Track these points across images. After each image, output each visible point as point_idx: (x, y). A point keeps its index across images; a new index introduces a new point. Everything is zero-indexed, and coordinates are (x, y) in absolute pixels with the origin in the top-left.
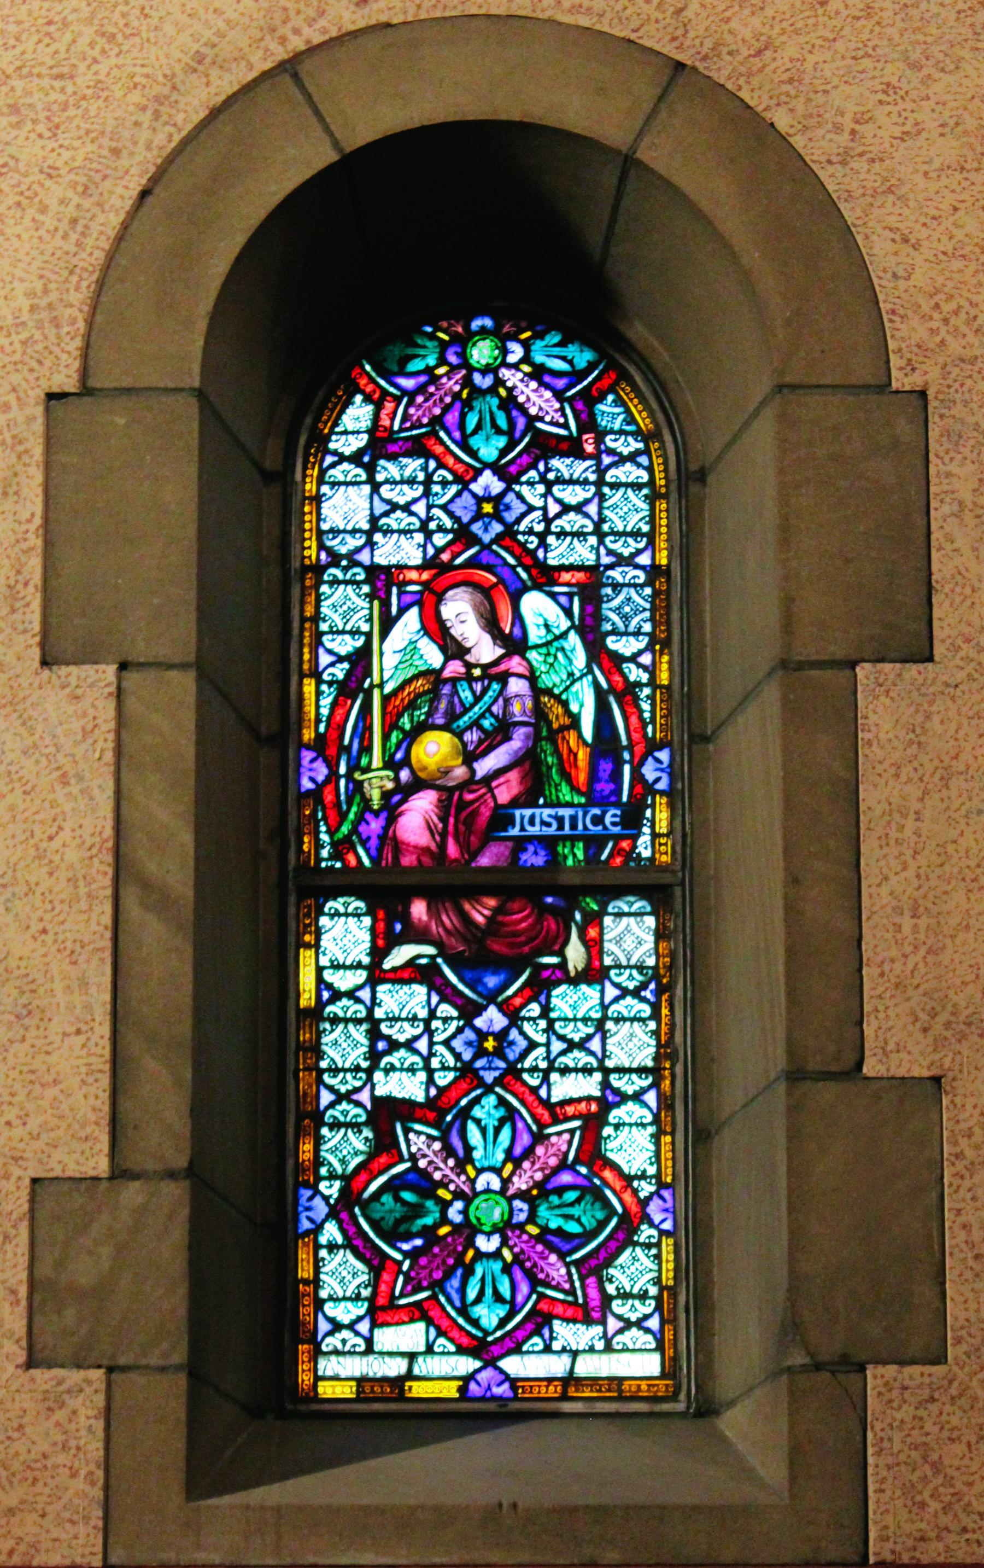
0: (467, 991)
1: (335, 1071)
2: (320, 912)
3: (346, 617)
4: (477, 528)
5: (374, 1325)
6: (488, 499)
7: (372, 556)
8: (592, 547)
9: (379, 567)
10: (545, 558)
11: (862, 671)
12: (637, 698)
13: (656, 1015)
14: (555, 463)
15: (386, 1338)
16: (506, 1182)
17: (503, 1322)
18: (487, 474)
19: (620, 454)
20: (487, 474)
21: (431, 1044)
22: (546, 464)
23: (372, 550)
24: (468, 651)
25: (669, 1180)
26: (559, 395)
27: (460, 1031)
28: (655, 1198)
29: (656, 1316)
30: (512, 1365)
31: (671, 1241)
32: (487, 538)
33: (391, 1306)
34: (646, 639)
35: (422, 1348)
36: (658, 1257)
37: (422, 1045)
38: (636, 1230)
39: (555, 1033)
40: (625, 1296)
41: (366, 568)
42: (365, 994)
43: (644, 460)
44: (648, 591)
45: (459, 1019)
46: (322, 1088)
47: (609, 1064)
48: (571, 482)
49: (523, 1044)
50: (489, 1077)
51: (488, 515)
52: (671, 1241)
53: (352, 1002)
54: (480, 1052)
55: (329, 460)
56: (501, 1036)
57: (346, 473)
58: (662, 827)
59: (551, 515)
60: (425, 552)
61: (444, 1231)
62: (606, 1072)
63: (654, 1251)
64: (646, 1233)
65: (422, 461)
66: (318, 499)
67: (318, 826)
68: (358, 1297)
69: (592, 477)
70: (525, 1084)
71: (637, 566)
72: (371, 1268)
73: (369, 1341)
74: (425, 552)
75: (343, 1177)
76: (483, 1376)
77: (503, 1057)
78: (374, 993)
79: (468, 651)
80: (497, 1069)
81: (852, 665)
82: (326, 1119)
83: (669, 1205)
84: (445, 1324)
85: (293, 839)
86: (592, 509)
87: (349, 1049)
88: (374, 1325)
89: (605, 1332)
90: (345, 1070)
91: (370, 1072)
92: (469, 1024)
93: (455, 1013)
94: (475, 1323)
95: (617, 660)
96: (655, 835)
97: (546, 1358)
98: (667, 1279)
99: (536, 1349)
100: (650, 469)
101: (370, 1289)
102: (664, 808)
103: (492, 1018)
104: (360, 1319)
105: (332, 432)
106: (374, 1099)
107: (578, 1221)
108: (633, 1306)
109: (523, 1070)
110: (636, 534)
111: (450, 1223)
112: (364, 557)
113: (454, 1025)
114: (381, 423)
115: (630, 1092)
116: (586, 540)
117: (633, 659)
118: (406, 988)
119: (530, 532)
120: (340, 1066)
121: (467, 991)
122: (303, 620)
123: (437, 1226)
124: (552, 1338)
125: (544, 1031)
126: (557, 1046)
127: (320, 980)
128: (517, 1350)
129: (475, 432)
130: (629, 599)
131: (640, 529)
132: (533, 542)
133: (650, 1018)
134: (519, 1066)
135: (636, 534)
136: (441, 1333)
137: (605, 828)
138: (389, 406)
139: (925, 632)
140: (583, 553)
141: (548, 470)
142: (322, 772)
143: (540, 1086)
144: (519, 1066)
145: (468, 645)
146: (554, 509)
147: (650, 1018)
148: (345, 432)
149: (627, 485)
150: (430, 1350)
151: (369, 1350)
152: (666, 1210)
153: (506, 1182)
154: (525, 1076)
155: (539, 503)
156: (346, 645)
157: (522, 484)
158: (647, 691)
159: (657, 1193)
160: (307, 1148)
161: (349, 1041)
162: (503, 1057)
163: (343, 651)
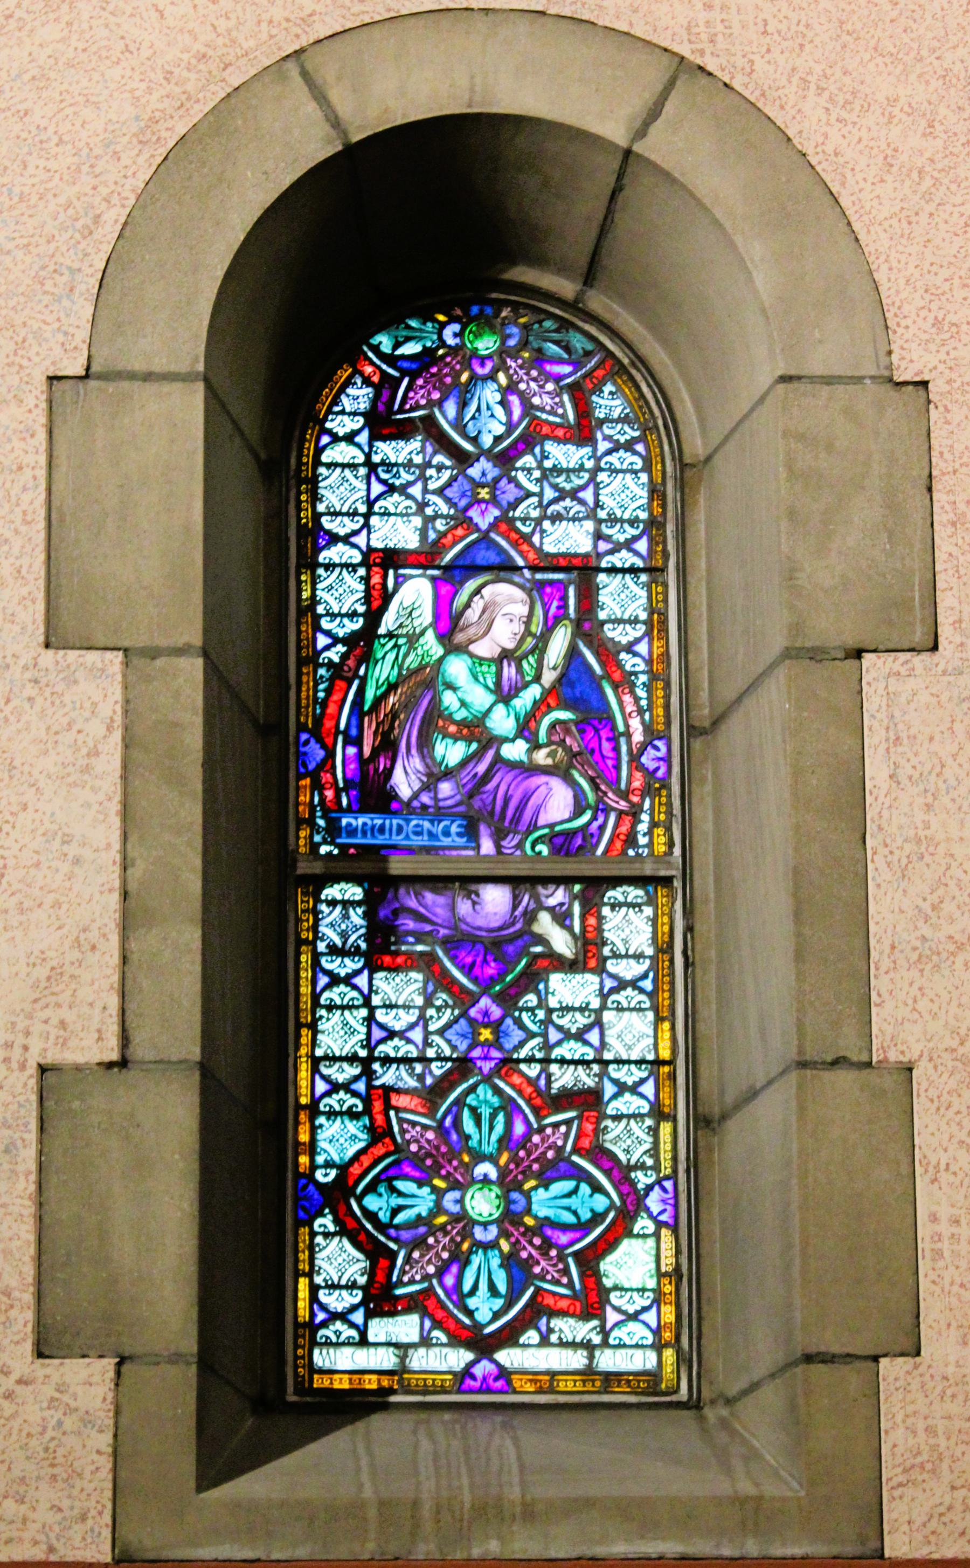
0: (464, 980)
3: (344, 935)
5: (369, 1315)
7: (369, 539)
10: (541, 543)
11: (884, 1362)
12: (633, 685)
13: (648, 468)
14: (556, 1323)
15: (379, 1329)
17: (496, 1316)
23: (369, 533)
25: (661, 727)
27: (453, 479)
28: (657, 1188)
29: (645, 539)
30: (506, 1357)
32: (484, 525)
34: (644, 628)
35: (415, 1338)
39: (552, 1022)
43: (640, 448)
47: (607, 1056)
50: (487, 1066)
53: (349, 989)
55: (325, 439)
56: (494, 485)
62: (605, 1063)
64: (643, 1224)
66: (313, 1027)
67: (315, 811)
72: (368, 1255)
73: (363, 1333)
76: (478, 1371)
77: (500, 1048)
78: (371, 980)
81: (876, 1359)
84: (440, 1314)
87: (344, 587)
88: (369, 1315)
89: (603, 1326)
90: (342, 616)
91: (367, 516)
92: (463, 472)
94: (470, 1313)
97: (545, 1351)
101: (365, 1277)
103: (483, 518)
104: (354, 1308)
105: (329, 411)
109: (518, 1061)
111: (446, 1212)
113: (446, 475)
118: (402, 976)
121: (464, 980)
122: (300, 942)
123: (433, 1214)
127: (314, 1298)
131: (644, 1163)
133: (642, 470)
136: (437, 1324)
139: (930, 559)
141: (551, 1330)
142: (320, 754)
143: (533, 533)
147: (642, 470)
148: (343, 412)
149: (629, 1117)
150: (425, 1341)
151: (363, 1341)
155: (535, 489)
157: (517, 470)
159: (659, 1182)
161: (346, 1029)
162: (500, 1048)
163: (341, 633)
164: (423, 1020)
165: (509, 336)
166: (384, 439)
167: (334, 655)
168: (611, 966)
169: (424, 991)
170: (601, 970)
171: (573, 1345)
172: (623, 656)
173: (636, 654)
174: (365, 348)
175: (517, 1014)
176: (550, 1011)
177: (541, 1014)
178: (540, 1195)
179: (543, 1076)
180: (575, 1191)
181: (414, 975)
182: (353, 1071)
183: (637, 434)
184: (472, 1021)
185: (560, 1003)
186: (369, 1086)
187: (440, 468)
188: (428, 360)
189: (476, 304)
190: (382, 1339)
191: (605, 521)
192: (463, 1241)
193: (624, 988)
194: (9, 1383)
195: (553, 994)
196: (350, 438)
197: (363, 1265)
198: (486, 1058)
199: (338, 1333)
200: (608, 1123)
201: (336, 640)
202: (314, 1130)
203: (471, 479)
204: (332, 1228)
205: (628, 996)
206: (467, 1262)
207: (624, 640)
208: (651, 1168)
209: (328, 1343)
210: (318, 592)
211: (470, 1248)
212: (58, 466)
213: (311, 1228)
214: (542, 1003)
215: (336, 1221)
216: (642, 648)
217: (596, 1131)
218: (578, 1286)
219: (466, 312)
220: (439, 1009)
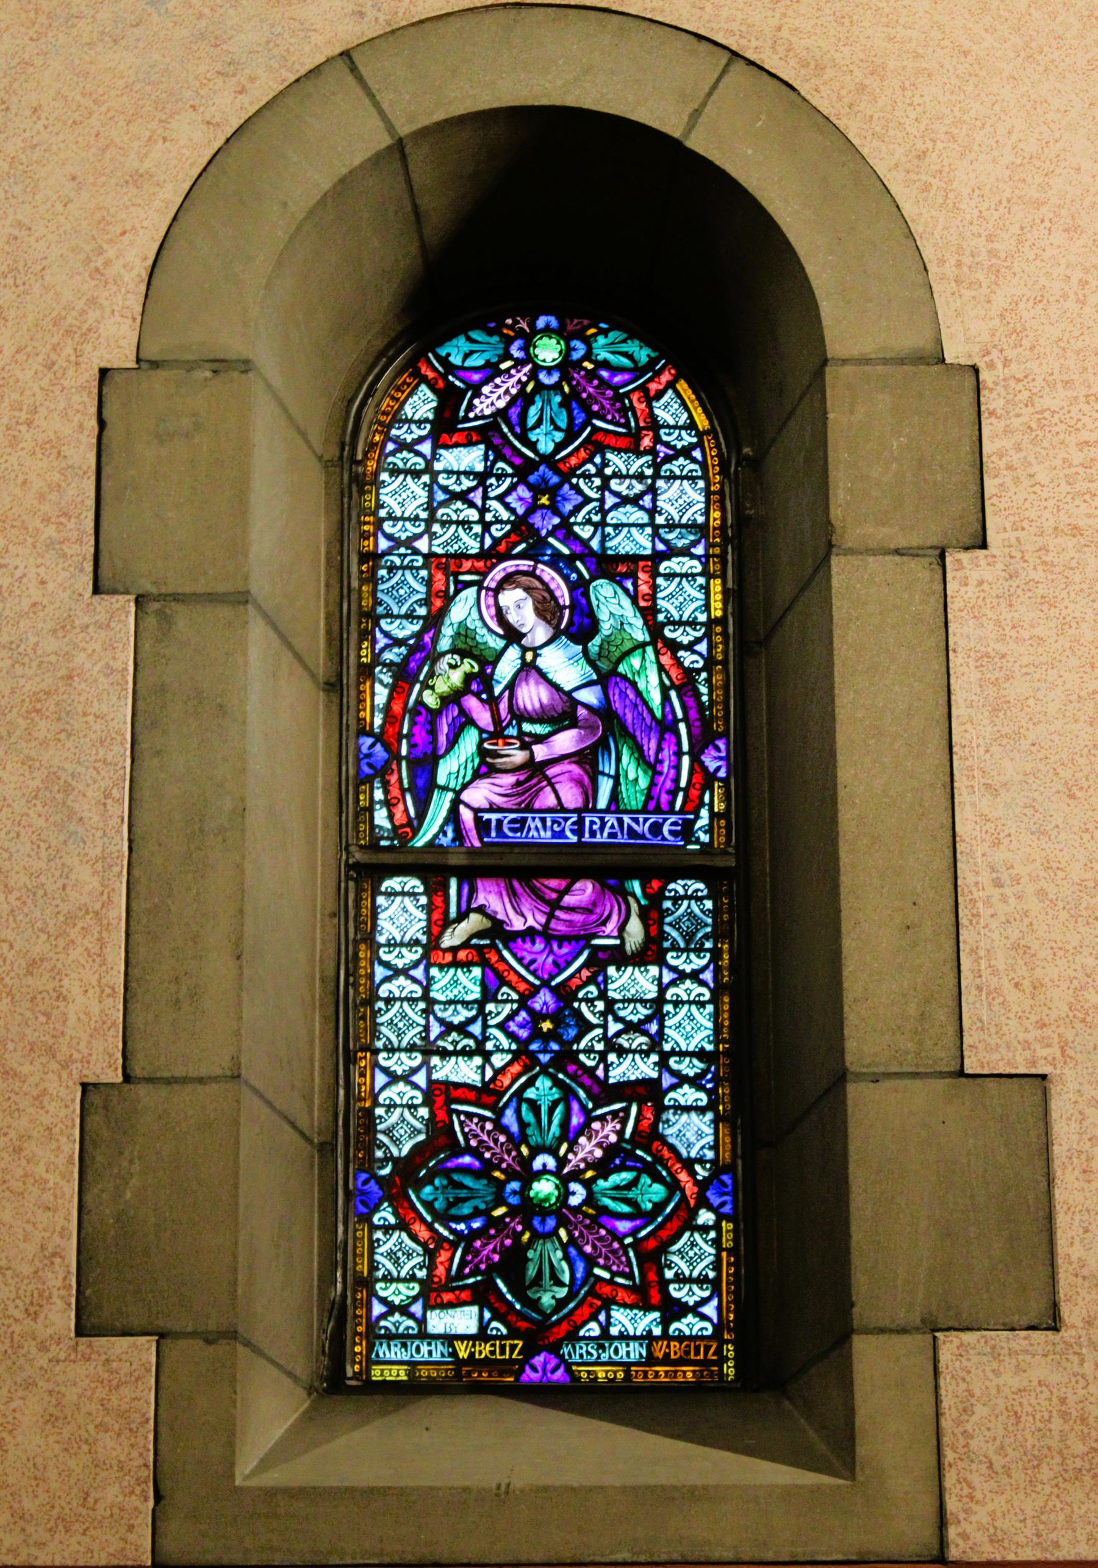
1: (391, 1050)
2: (375, 892)
5: (426, 1307)
9: (435, 555)
15: (438, 1322)
16: (562, 1162)
19: (673, 448)
21: (485, 1026)
22: (603, 458)
24: (524, 635)
31: (723, 822)
37: (476, 1029)
38: (694, 1214)
41: (425, 556)
42: (417, 1309)
46: (377, 1071)
50: (544, 1058)
51: (543, 506)
52: (723, 822)
54: (536, 1034)
57: (400, 956)
59: (607, 507)
60: (482, 542)
63: (712, 1234)
68: (412, 1278)
70: (582, 1065)
71: (693, 557)
73: (422, 1322)
74: (482, 542)
79: (524, 635)
80: (552, 1051)
83: (723, 754)
88: (426, 1307)
95: (674, 646)
96: (713, 815)
99: (593, 1334)
100: (703, 465)
106: (430, 1081)
110: (701, 1281)
112: (422, 545)
115: (688, 982)
117: (690, 647)
119: (589, 1051)
120: (396, 1045)
124: (609, 1323)
125: (599, 488)
126: (614, 1027)
129: (534, 428)
130: (687, 1038)
134: (575, 1047)
135: (701, 1281)
137: (664, 839)
138: (444, 1256)
140: (646, 1068)
144: (575, 1047)
145: (524, 630)
151: (424, 1335)
152: (720, 758)
153: (562, 1162)
154: (582, 1057)
156: (406, 630)
158: (704, 675)
164: (482, 1014)
166: (447, 447)
170: (662, 963)
173: (694, 652)
174: (430, 355)
175: (576, 1005)
177: (600, 1006)
179: (601, 1066)
183: (695, 440)
184: (531, 1011)
188: (490, 372)
191: (663, 526)
192: (503, 1171)
198: (545, 1051)
202: (624, 1337)
205: (687, 989)
206: (605, 1208)
207: (685, 640)
211: (591, 362)
212: (682, 1555)
214: (603, 995)
215: (395, 1214)
216: (702, 647)
217: (657, 1119)
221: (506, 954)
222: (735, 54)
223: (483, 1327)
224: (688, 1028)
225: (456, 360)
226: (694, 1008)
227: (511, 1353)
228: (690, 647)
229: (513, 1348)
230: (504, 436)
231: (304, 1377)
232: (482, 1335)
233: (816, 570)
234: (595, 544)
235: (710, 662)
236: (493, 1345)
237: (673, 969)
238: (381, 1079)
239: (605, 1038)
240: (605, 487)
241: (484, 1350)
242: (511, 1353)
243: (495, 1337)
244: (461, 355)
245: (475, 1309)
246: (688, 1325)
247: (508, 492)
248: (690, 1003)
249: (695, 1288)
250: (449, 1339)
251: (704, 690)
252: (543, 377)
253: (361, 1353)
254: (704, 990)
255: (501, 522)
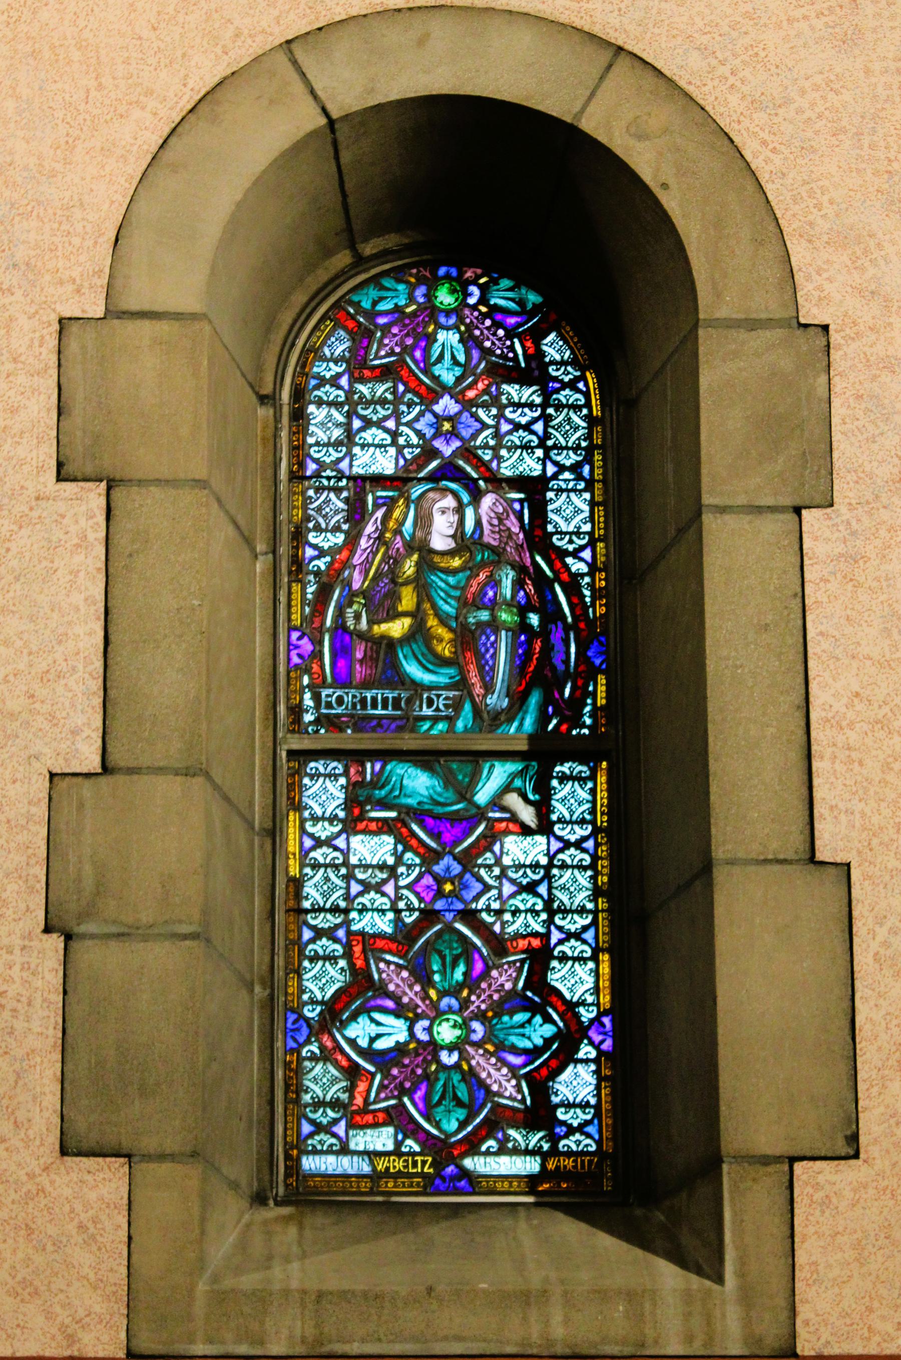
3: (326, 896)
4: (438, 444)
6: (450, 419)
8: (539, 459)
15: (361, 1140)
18: (447, 398)
20: (447, 398)
26: (513, 1069)
33: (365, 1110)
36: (593, 792)
40: (569, 1106)
44: (587, 496)
45: (421, 404)
48: (519, 405)
49: (479, 887)
54: (438, 434)
58: (601, 701)
61: (412, 1046)
65: (389, 384)
69: (538, 400)
75: (322, 1003)
82: (307, 953)
85: (280, 1036)
86: (543, 889)
93: (418, 861)
98: (602, 822)
100: (587, 395)
102: (604, 772)
107: (529, 1038)
108: (578, 1146)
114: (355, 1102)
116: (533, 453)
118: (376, 839)
119: (486, 446)
125: (495, 416)
128: (477, 1152)
132: (487, 456)
140: (531, 466)
146: (505, 427)
151: (344, 1150)
158: (587, 579)
160: (293, 984)
165: (471, 295)
167: (321, 564)
168: (557, 829)
169: (395, 853)
171: (527, 1152)
172: (569, 560)
176: (504, 870)
178: (403, 1037)
180: (372, 1040)
181: (385, 838)
182: (334, 920)
184: (436, 877)
185: (513, 860)
186: (349, 933)
187: (410, 405)
189: (444, 265)
190: (361, 1148)
193: (568, 848)
194: (896, 766)
195: (507, 854)
196: (334, 382)
197: (344, 1084)
199: (321, 1142)
200: (554, 963)
201: (322, 553)
203: (435, 415)
204: (582, 1010)
205: (570, 856)
208: (592, 1004)
209: (315, 1152)
210: (304, 799)
213: (599, 1009)
216: (587, 554)
218: (528, 1102)
219: (434, 273)
220: (409, 867)
221: (415, 827)
222: (620, 49)
223: (398, 1144)
224: (572, 801)
225: (366, 304)
226: (576, 871)
227: (423, 1167)
228: (575, 554)
229: (424, 1163)
230: (411, 371)
231: (244, 1182)
232: (397, 1152)
233: (681, 531)
234: (497, 928)
235: (593, 568)
236: (406, 1161)
237: (559, 839)
238: (306, 1128)
239: (500, 896)
240: (500, 416)
241: (398, 1164)
242: (423, 1167)
243: (409, 1154)
244: (370, 302)
245: (391, 1130)
246: (570, 1143)
247: (416, 419)
248: (573, 867)
249: (576, 917)
250: (372, 1155)
251: (587, 593)
252: (454, 1003)
253: (293, 994)
254: (586, 947)
255: (412, 446)
